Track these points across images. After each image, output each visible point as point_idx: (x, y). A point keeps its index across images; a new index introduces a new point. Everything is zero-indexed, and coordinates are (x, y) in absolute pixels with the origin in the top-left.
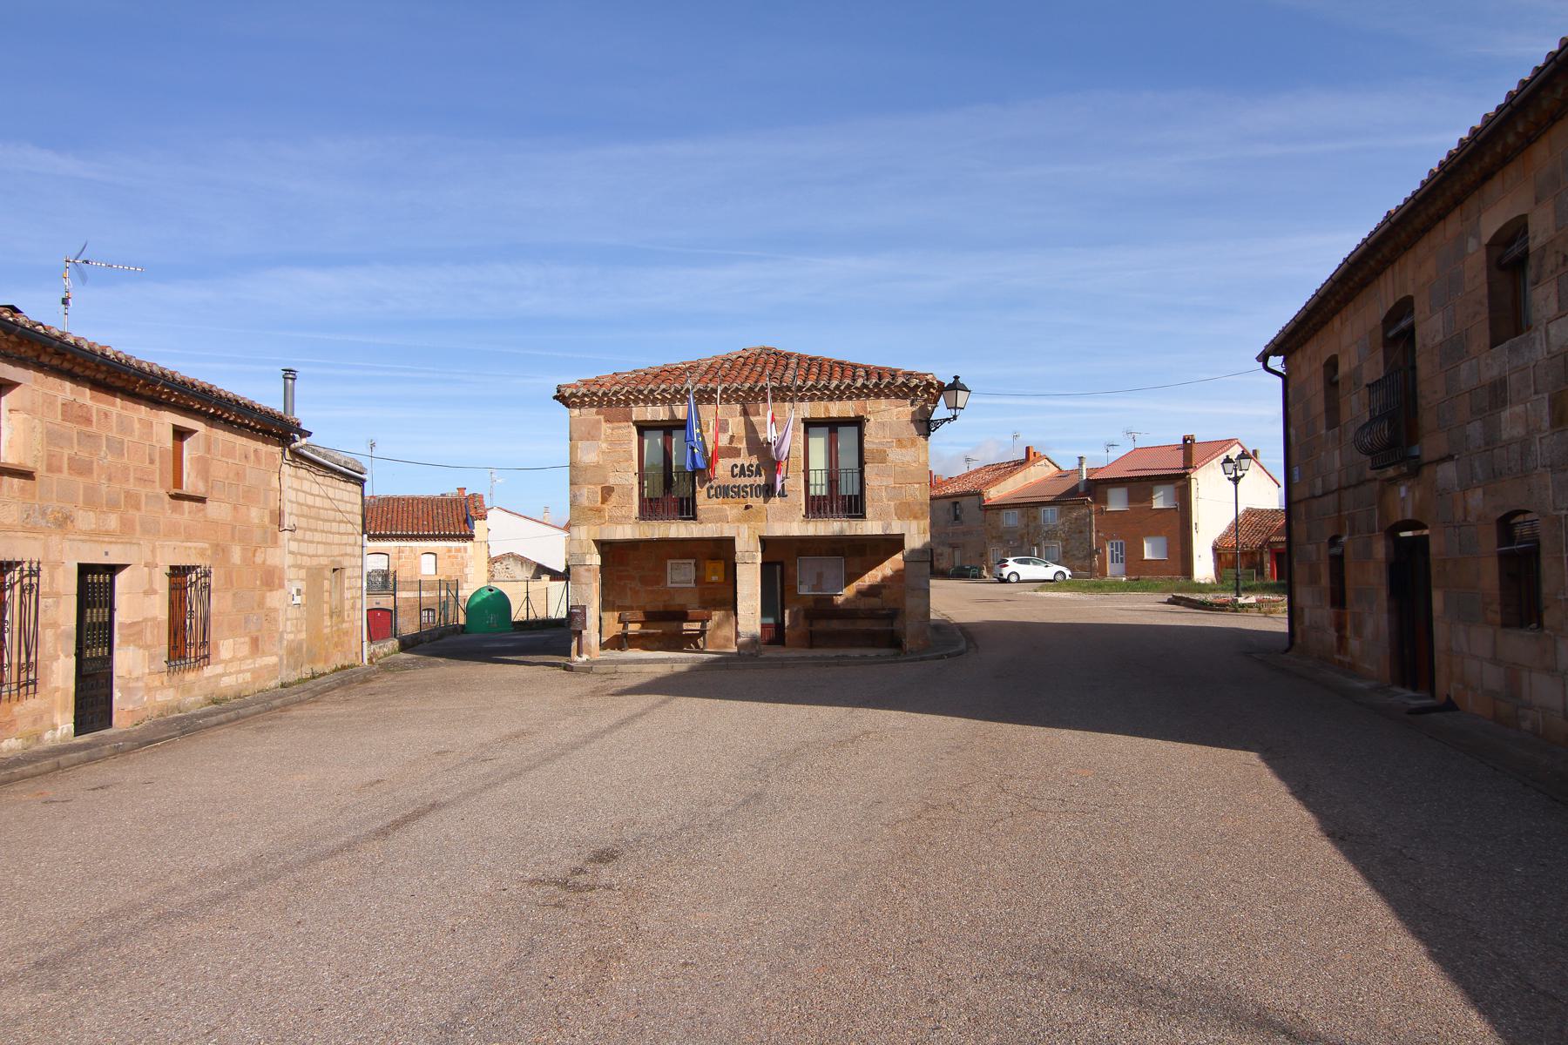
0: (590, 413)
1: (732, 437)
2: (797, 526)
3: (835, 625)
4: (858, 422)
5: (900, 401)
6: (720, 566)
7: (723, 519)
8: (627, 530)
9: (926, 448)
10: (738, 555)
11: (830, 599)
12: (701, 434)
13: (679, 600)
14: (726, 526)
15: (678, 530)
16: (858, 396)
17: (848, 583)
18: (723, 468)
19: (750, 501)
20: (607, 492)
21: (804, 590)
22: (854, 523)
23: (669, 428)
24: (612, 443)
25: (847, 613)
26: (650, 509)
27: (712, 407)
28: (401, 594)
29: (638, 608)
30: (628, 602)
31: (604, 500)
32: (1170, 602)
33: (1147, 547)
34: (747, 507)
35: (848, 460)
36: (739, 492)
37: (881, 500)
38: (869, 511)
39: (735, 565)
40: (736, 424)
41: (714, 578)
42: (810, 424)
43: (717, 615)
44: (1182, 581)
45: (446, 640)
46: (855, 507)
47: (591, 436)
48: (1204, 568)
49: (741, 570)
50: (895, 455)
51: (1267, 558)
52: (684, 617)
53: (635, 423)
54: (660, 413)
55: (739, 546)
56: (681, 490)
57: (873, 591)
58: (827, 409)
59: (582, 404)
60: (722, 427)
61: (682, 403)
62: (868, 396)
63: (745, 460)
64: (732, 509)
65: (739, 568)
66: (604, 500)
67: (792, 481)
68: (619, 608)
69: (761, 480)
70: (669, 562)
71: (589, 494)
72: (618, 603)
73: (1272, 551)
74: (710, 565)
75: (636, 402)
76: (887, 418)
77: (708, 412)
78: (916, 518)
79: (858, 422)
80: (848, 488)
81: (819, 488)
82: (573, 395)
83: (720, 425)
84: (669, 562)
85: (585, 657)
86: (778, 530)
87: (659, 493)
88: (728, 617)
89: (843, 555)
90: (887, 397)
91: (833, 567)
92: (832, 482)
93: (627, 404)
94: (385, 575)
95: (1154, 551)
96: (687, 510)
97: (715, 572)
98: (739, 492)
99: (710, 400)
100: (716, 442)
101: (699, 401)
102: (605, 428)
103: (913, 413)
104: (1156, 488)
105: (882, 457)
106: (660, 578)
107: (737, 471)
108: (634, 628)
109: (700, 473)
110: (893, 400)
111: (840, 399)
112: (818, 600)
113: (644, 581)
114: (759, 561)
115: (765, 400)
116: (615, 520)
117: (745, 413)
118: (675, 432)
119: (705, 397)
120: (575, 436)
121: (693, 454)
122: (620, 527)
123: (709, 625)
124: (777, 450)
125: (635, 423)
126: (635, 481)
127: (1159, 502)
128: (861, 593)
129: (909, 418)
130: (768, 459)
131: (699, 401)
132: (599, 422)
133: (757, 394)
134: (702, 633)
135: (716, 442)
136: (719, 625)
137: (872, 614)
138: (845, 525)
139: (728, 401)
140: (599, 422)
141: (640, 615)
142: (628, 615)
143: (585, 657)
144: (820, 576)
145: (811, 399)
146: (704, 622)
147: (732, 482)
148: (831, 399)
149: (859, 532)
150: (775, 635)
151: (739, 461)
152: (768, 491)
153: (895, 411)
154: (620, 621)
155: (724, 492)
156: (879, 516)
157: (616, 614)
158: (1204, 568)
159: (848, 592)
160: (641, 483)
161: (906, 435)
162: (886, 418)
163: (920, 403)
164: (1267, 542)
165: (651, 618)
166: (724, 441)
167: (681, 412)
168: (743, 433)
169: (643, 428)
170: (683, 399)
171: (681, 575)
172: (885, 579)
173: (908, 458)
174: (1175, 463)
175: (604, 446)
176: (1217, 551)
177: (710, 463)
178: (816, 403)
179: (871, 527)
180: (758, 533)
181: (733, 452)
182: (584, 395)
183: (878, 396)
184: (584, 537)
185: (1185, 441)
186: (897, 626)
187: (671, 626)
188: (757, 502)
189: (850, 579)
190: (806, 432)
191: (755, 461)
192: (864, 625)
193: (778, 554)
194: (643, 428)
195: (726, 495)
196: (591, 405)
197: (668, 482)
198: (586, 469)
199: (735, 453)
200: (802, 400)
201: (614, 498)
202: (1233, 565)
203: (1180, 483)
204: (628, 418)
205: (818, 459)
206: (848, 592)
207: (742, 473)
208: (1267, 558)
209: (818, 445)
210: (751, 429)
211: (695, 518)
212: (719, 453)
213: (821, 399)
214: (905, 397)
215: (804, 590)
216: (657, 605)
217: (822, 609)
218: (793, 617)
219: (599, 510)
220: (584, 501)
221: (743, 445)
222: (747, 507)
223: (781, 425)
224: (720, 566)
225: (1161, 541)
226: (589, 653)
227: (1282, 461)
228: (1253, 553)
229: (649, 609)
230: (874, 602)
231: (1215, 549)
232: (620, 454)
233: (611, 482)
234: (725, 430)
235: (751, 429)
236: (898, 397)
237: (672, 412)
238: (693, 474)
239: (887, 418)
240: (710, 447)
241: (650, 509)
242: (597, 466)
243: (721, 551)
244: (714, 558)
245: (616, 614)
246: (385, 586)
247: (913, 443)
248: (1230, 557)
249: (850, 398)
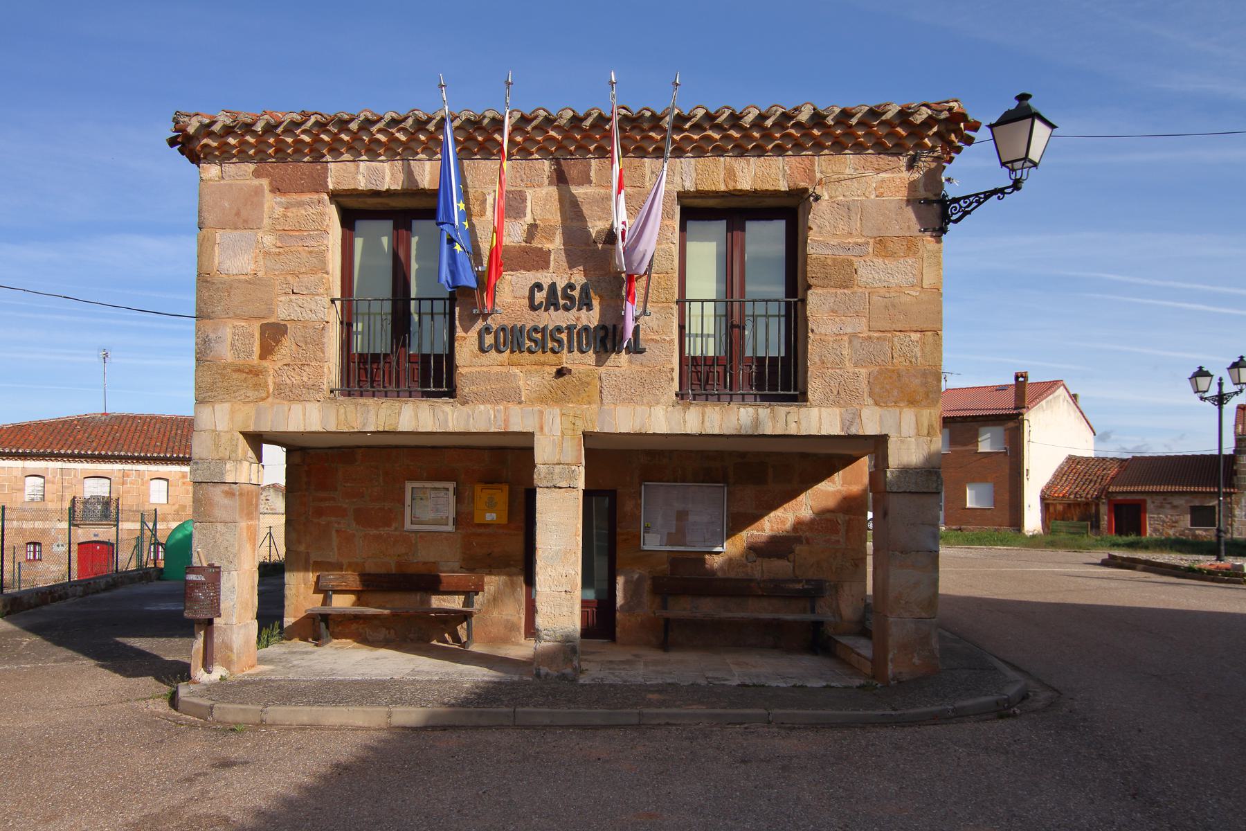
0: (241, 174)
1: (533, 228)
2: (662, 416)
3: (707, 608)
4: (790, 209)
5: (885, 160)
6: (501, 496)
7: (510, 396)
8: (313, 417)
9: (936, 256)
10: (540, 472)
11: (699, 559)
12: (468, 214)
13: (425, 555)
14: (515, 409)
15: (416, 417)
16: (799, 147)
17: (733, 530)
18: (512, 290)
19: (567, 359)
20: (273, 334)
21: (652, 543)
22: (782, 410)
23: (410, 211)
24: (283, 234)
25: (729, 586)
26: (362, 374)
27: (492, 165)
28: (124, 526)
29: (351, 566)
30: (333, 557)
31: (266, 352)
32: (1104, 563)
33: (970, 494)
34: (560, 373)
35: (767, 286)
36: (545, 340)
37: (840, 364)
38: (815, 387)
39: (531, 495)
40: (541, 201)
41: (490, 517)
42: (694, 210)
43: (492, 583)
44: (1007, 531)
45: (121, 591)
46: (783, 379)
47: (242, 221)
48: (1033, 520)
49: (543, 500)
50: (872, 271)
51: (1104, 509)
52: (432, 584)
53: (335, 196)
54: (382, 175)
55: (543, 453)
56: (427, 338)
57: (777, 547)
58: (731, 174)
59: (224, 155)
60: (512, 206)
61: (431, 155)
62: (818, 147)
63: (558, 274)
64: (529, 375)
65: (542, 498)
66: (266, 352)
67: (647, 317)
68: (318, 566)
69: (591, 317)
70: (409, 486)
71: (234, 339)
72: (314, 557)
73: (1110, 502)
74: (482, 494)
75: (334, 150)
76: (857, 194)
77: (486, 178)
78: (912, 402)
79: (790, 209)
80: (766, 340)
81: (707, 346)
82: (206, 130)
83: (505, 203)
84: (409, 486)
85: (218, 672)
86: (625, 420)
87: (382, 345)
88: (513, 586)
89: (724, 479)
90: (859, 148)
91: (704, 506)
92: (732, 327)
93: (318, 158)
94: (106, 502)
95: (978, 498)
96: (438, 378)
97: (491, 506)
98: (545, 340)
99: (489, 149)
100: (498, 231)
101: (465, 152)
102: (272, 204)
103: (912, 186)
104: (982, 430)
105: (844, 276)
106: (390, 512)
107: (540, 297)
108: (343, 602)
109: (465, 300)
110: (871, 158)
111: (760, 151)
112: (677, 560)
113: (363, 518)
114: (581, 485)
115: (603, 152)
116: (288, 394)
117: (560, 178)
118: (417, 225)
119: (479, 138)
120: (210, 219)
121: (453, 253)
122: (297, 408)
123: (479, 599)
124: (628, 252)
125: (335, 196)
126: (333, 316)
127: (986, 443)
128: (757, 551)
129: (903, 194)
130: (606, 271)
131: (465, 152)
132: (258, 191)
133: (587, 135)
134: (465, 616)
135: (498, 231)
136: (495, 600)
137: (775, 590)
138: (764, 412)
139: (525, 153)
140: (258, 191)
141: (353, 580)
142: (332, 578)
143: (218, 672)
144: (682, 516)
145: (699, 152)
146: (469, 595)
147: (530, 320)
148: (741, 151)
149: (793, 430)
150: (600, 620)
151: (545, 278)
152: (608, 339)
153: (874, 179)
154: (317, 590)
155: (512, 340)
156: (837, 397)
157: (312, 577)
158: (1033, 520)
159: (732, 547)
160: (347, 326)
161: (894, 230)
162: (852, 192)
163: (926, 163)
164: (1104, 492)
165: (372, 585)
166: (514, 235)
167: (426, 174)
168: (553, 216)
169: (355, 210)
170: (434, 146)
171: (430, 509)
172: (799, 525)
173: (898, 279)
174: (1005, 403)
175: (269, 240)
176: (1046, 502)
177: (486, 284)
178: (708, 161)
179: (818, 419)
180: (581, 426)
181: (534, 258)
182: (228, 130)
183: (839, 147)
184: (222, 425)
185: (1017, 377)
186: (823, 612)
187: (406, 602)
188: (581, 362)
189: (738, 523)
190: (683, 228)
191: (579, 278)
192: (763, 610)
193: (621, 474)
194: (355, 210)
195: (517, 347)
196: (243, 156)
197: (401, 323)
198: (229, 287)
199: (539, 260)
200: (679, 152)
201: (287, 348)
202: (1063, 517)
203: (1011, 424)
204: (318, 185)
205: (704, 281)
206: (732, 547)
207: (552, 302)
208: (1104, 509)
209: (705, 255)
210: (572, 211)
211: (451, 393)
212: (501, 260)
213: (719, 151)
214: (897, 149)
215: (652, 543)
216: (385, 561)
217: (683, 578)
218: (633, 590)
219: (255, 372)
220: (225, 352)
221: (556, 245)
222: (560, 373)
223: (637, 202)
224: (501, 496)
225: (987, 488)
226: (228, 664)
227: (539, 517)
228: (1087, 504)
229: (371, 568)
230: (779, 567)
231: (1043, 499)
232: (295, 255)
233: (283, 311)
234: (519, 213)
235: (572, 211)
236: (881, 149)
237: (409, 174)
238: (452, 299)
239: (857, 194)
240: (485, 248)
241: (362, 374)
242: (253, 281)
243: (505, 466)
244: (491, 479)
245: (312, 577)
246: (105, 515)
247: (910, 246)
248: (1060, 508)
249: (780, 151)
